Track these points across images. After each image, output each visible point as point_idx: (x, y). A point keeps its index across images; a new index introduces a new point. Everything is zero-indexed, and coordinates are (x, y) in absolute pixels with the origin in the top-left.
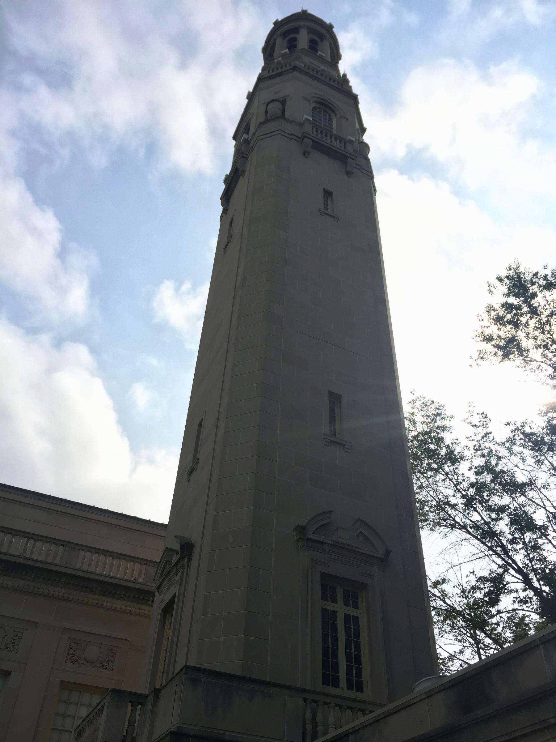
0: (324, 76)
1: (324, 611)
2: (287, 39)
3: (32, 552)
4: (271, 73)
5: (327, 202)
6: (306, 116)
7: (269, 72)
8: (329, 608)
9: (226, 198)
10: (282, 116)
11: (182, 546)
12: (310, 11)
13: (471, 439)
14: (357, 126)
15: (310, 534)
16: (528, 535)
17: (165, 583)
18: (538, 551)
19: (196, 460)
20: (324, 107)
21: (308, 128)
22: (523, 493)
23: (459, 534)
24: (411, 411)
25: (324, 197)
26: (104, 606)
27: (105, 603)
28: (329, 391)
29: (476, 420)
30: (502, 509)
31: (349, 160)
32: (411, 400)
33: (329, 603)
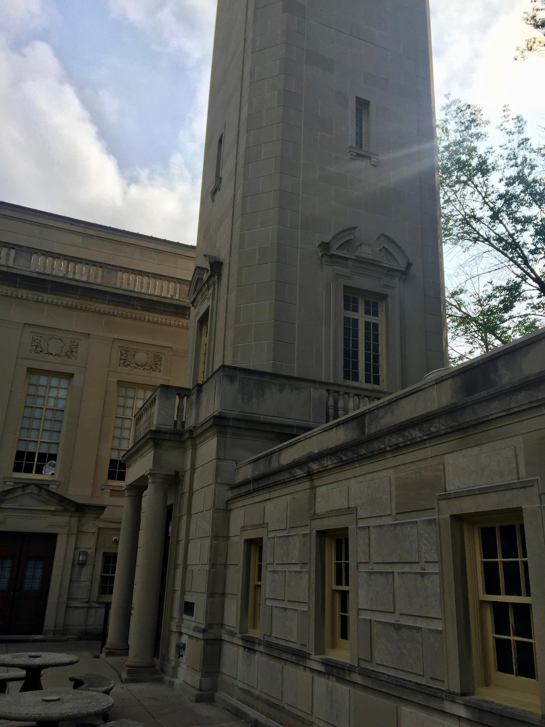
1: (346, 319)
8: (352, 317)
11: (211, 265)
13: (505, 147)
15: (334, 251)
19: (219, 179)
30: (528, 220)
32: (444, 105)
33: (351, 312)
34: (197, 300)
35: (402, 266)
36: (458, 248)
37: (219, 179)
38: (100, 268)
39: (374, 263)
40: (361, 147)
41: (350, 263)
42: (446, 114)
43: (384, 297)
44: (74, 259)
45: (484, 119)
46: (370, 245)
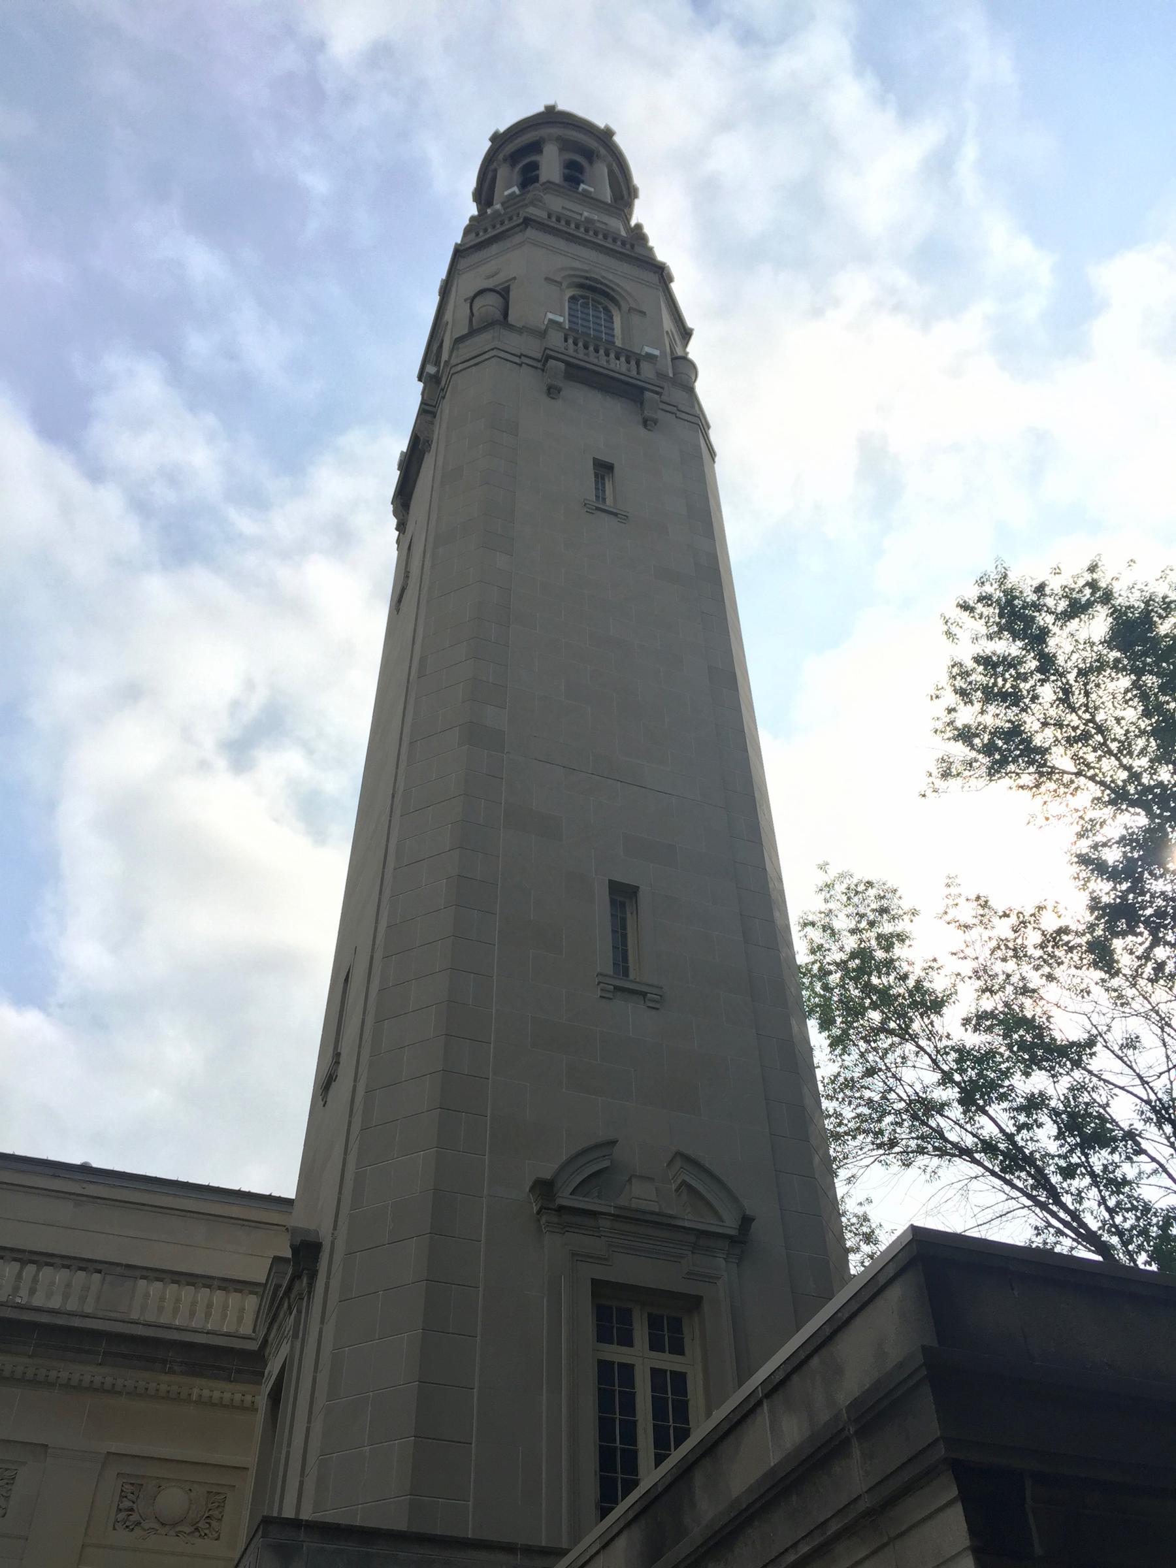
0: (591, 233)
1: (605, 1368)
2: (520, 166)
3: (32, 1291)
4: (483, 237)
5: (604, 484)
6: (550, 316)
7: (477, 235)
8: (617, 1359)
9: (403, 498)
10: (503, 320)
11: (295, 1249)
12: (562, 106)
13: (962, 955)
14: (668, 324)
15: (565, 1198)
16: (1099, 1159)
17: (272, 1336)
18: (1127, 1189)
19: (337, 1055)
20: (593, 294)
21: (555, 340)
22: (1077, 1064)
23: (963, 1167)
24: (824, 907)
25: (596, 475)
26: (194, 1398)
27: (196, 1391)
28: (610, 881)
29: (967, 912)
30: (1034, 1103)
31: (648, 394)
32: (821, 884)
33: (615, 1347)
34: (270, 1340)
35: (730, 1224)
36: (913, 1171)
37: (337, 1055)
38: (79, 1272)
39: (665, 1220)
40: (626, 973)
41: (604, 1223)
42: (826, 901)
43: (694, 1303)
44: (35, 1258)
45: (906, 905)
46: (652, 1179)
